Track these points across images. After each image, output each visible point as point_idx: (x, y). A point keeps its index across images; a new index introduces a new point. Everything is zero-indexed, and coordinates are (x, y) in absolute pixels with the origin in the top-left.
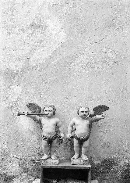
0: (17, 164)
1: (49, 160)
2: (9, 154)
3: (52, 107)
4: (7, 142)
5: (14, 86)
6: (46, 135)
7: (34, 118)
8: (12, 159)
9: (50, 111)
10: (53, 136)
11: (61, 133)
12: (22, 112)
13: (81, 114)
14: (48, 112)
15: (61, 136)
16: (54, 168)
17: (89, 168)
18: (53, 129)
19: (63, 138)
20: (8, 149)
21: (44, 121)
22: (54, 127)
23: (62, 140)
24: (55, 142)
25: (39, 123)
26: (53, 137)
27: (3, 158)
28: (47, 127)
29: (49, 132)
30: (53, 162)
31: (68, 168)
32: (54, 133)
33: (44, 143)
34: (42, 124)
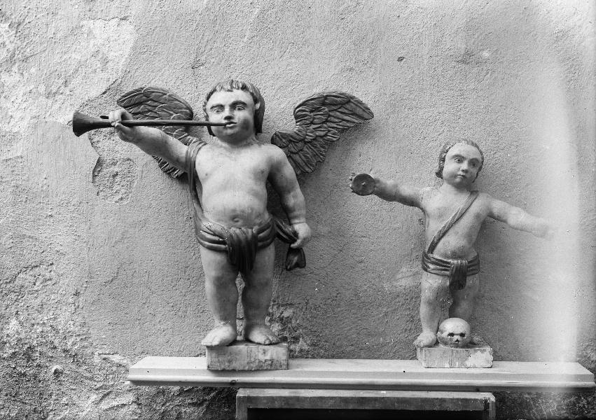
0: (130, 397)
1: (242, 348)
2: (89, 351)
3: (244, 88)
4: (77, 294)
5: (99, 23)
6: (217, 227)
7: (157, 149)
8: (100, 375)
9: (234, 106)
10: (255, 229)
11: (296, 217)
12: (94, 117)
13: (450, 167)
14: (227, 112)
15: (296, 234)
16: (307, 406)
17: (486, 402)
18: (256, 194)
19: (305, 240)
20: (83, 325)
21: (211, 159)
22: (261, 189)
23: (298, 251)
24: (268, 256)
25: (187, 177)
26: (254, 237)
27: (59, 367)
28: (225, 187)
29: (234, 211)
30: (262, 357)
31: (378, 406)
32: (259, 215)
33: (210, 262)
34: (201, 175)
